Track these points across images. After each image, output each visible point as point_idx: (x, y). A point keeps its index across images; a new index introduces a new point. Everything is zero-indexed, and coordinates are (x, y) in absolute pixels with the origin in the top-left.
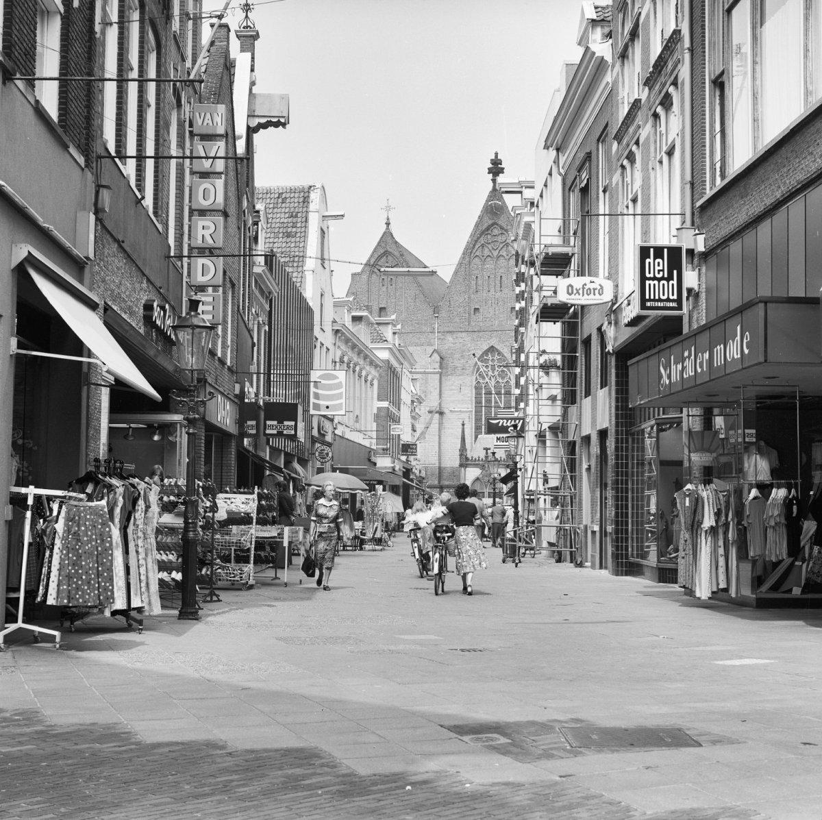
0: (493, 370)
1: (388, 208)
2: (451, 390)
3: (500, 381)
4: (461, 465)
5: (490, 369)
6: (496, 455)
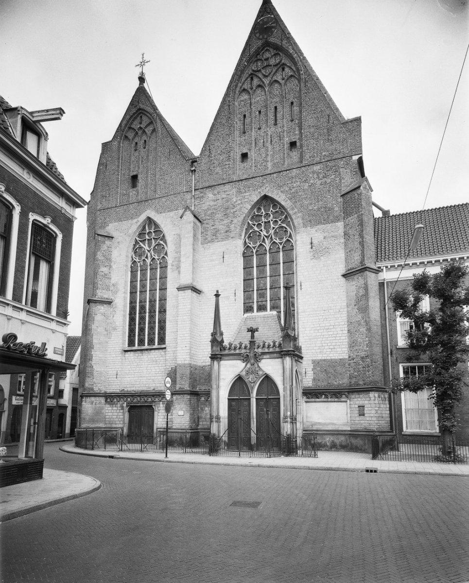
0: (267, 228)
1: (142, 64)
2: (212, 261)
3: (278, 241)
4: (214, 357)
5: (263, 228)
6: (256, 334)
